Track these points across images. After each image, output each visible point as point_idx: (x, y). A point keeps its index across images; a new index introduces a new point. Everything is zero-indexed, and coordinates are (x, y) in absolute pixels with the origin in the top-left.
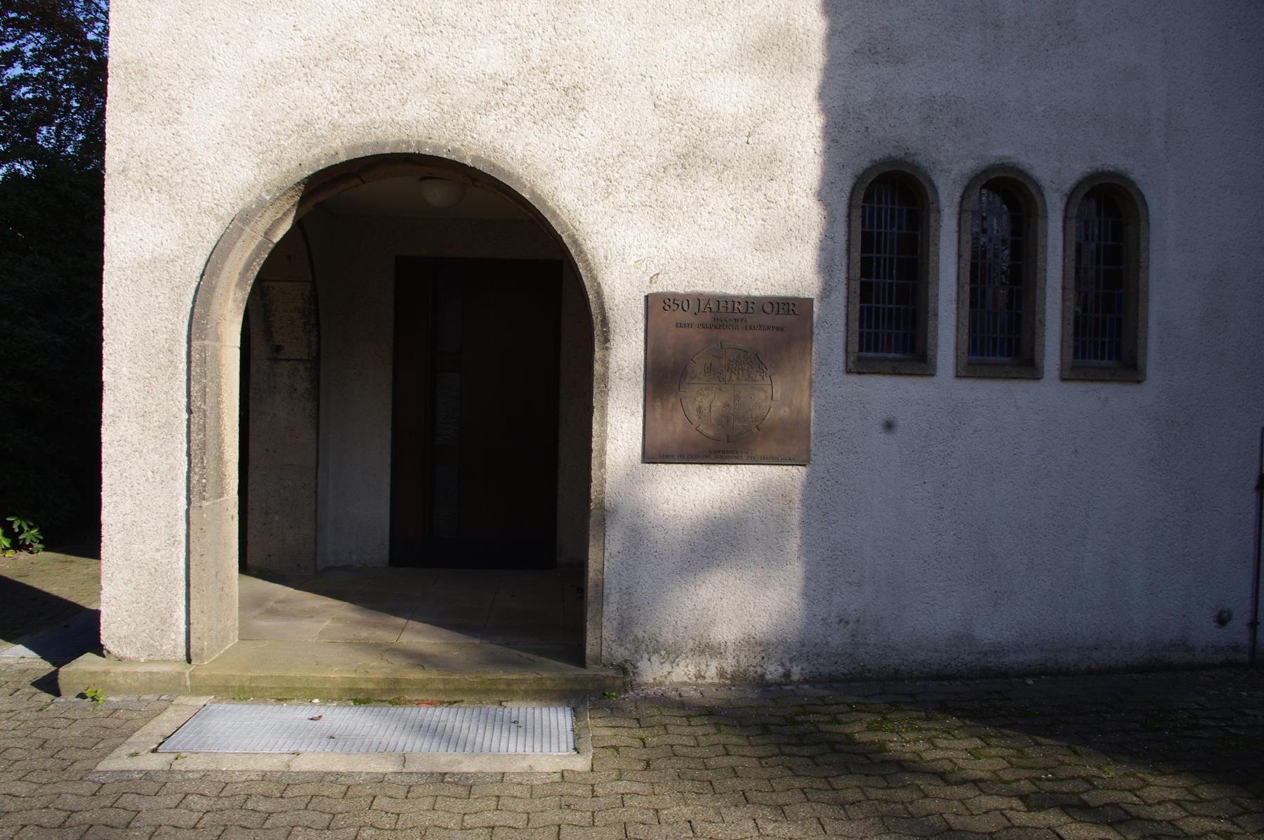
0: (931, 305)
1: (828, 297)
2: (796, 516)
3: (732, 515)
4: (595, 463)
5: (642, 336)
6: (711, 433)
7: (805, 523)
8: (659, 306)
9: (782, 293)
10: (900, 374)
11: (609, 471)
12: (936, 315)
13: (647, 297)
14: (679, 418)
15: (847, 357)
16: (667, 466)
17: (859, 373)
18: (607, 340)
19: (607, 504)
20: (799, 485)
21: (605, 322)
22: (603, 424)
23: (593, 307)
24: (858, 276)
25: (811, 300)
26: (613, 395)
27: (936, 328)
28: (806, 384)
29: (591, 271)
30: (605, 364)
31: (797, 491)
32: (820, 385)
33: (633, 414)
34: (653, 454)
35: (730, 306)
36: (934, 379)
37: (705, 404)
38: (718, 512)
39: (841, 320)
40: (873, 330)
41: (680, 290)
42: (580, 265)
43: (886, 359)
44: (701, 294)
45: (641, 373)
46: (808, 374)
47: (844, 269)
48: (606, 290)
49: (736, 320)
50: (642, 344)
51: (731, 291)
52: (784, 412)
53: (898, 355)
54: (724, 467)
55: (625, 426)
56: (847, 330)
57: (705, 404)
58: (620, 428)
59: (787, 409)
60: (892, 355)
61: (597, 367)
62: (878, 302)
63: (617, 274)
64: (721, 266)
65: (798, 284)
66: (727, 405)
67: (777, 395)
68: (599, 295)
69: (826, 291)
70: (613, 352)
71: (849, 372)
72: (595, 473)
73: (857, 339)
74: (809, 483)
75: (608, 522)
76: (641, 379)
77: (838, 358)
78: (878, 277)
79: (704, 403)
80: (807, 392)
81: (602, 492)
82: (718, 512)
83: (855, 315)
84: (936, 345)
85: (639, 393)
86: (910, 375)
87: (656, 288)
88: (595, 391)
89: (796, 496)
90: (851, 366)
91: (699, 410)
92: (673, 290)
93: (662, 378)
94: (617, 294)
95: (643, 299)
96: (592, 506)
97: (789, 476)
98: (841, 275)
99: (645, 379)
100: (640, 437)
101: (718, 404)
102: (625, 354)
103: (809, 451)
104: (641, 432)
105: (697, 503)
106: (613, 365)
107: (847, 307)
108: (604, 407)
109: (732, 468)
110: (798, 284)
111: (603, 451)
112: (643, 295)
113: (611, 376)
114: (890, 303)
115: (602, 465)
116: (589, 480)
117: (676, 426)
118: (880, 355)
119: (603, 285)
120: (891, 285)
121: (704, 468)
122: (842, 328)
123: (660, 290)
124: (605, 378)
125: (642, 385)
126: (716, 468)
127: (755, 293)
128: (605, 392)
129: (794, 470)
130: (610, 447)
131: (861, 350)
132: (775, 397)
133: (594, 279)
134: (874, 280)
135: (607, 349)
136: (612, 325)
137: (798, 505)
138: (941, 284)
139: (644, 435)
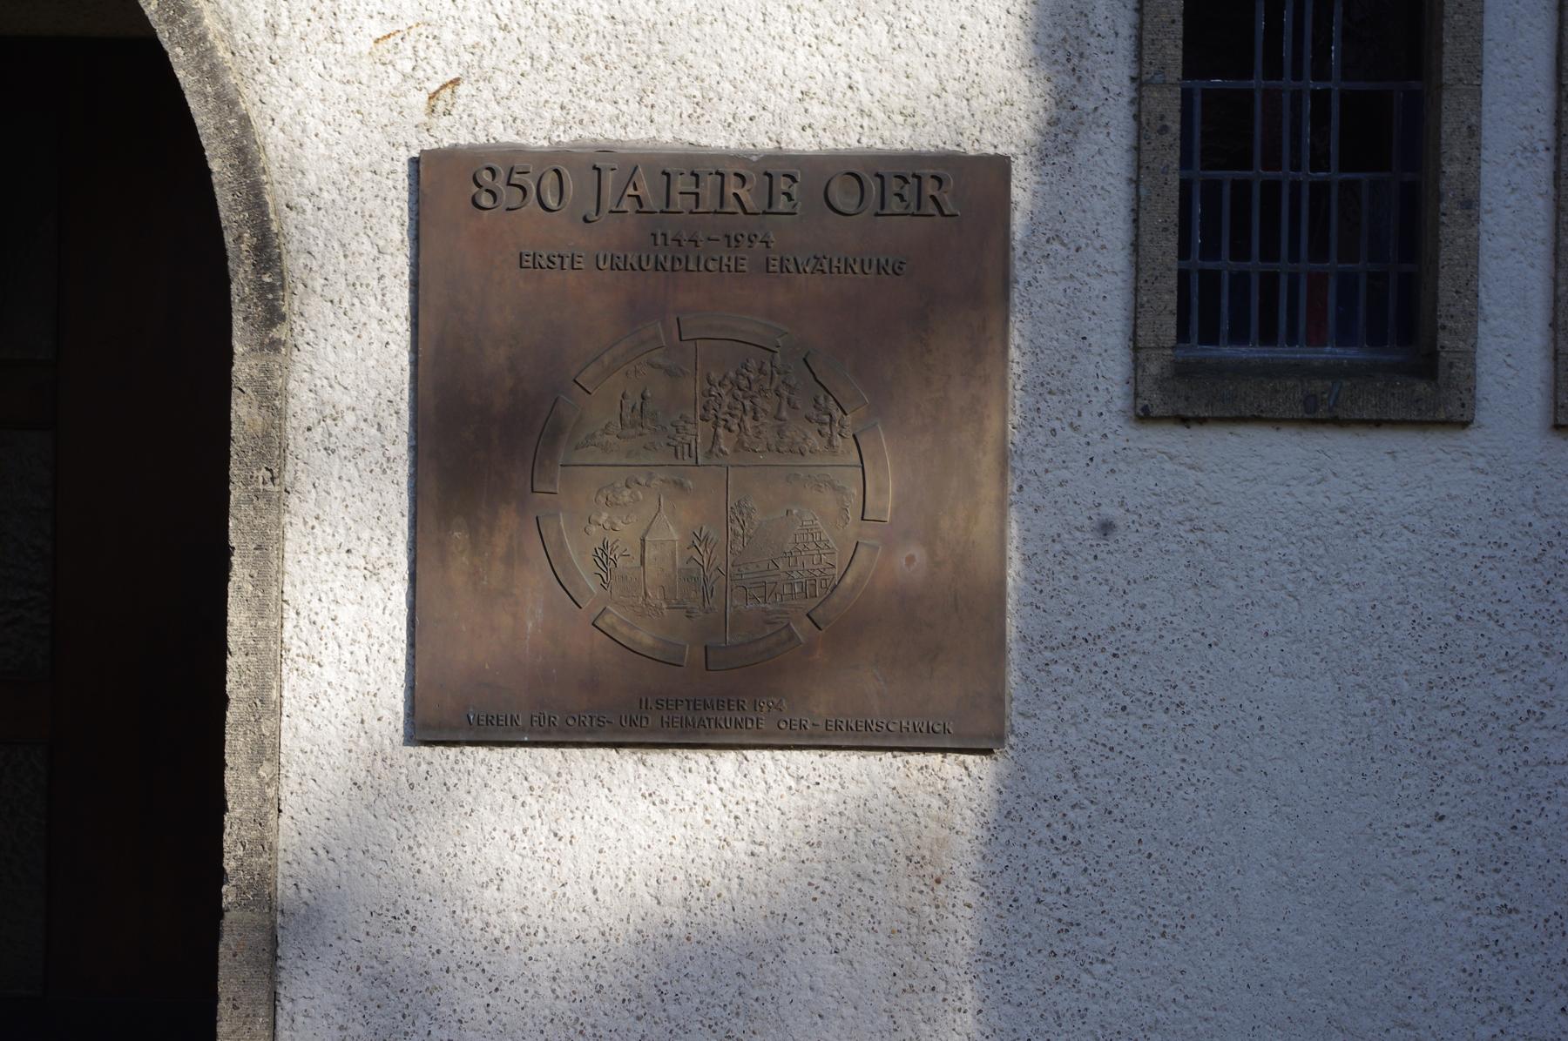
0: (1451, 169)
1: (1067, 149)
2: (962, 924)
3: (727, 929)
4: (236, 746)
5: (401, 300)
6: (645, 637)
7: (994, 962)
8: (459, 195)
9: (899, 138)
10: (1337, 422)
11: (292, 771)
12: (1470, 204)
13: (415, 162)
14: (534, 582)
15: (1137, 364)
16: (495, 755)
17: (1185, 421)
18: (274, 316)
19: (284, 890)
20: (968, 823)
21: (267, 252)
22: (269, 606)
23: (224, 199)
24: (1175, 72)
25: (999, 167)
26: (300, 508)
27: (1472, 252)
28: (987, 461)
29: (214, 73)
30: (272, 399)
31: (962, 844)
32: (1049, 457)
33: (372, 572)
34: (452, 709)
35: (709, 182)
36: (1470, 439)
37: (626, 532)
38: (676, 915)
39: (1117, 232)
40: (1255, 266)
41: (537, 136)
42: (179, 57)
43: (1270, 371)
44: (606, 151)
45: (399, 428)
46: (993, 425)
47: (1125, 46)
48: (273, 141)
49: (731, 241)
50: (403, 327)
51: (716, 138)
52: (909, 562)
53: (1350, 354)
54: (699, 758)
55: (347, 614)
56: (1137, 268)
57: (626, 532)
58: (328, 616)
59: (919, 553)
60: (1330, 353)
61: (243, 411)
62: (1296, 167)
63: (311, 82)
64: (679, 48)
65: (958, 107)
66: (698, 540)
67: (885, 502)
68: (246, 157)
69: (1061, 132)
70: (302, 358)
71: (1144, 417)
72: (237, 781)
73: (1171, 301)
74: (1008, 817)
75: (287, 951)
76: (401, 449)
77: (1107, 366)
78: (1273, 69)
79: (626, 533)
80: (989, 491)
81: (264, 846)
82: (676, 915)
83: (1167, 209)
84: (1473, 315)
85: (396, 498)
86: (1378, 424)
87: (452, 133)
88: (236, 493)
89: (962, 854)
90: (1154, 398)
91: (603, 556)
92: (507, 136)
93: (478, 444)
94: (313, 152)
95: (402, 170)
96: (229, 894)
97: (954, 784)
98: (1114, 71)
99: (415, 449)
100: (400, 652)
101: (669, 534)
102: (338, 364)
103: (999, 699)
104: (403, 635)
105: (603, 884)
106: (301, 401)
107: (1136, 182)
108: (268, 548)
109: (727, 761)
110: (958, 107)
111: (267, 705)
112: (404, 156)
113: (297, 441)
114: (1319, 162)
115: (266, 751)
116: (216, 804)
117: (526, 616)
118: (1281, 353)
119: (259, 124)
120: (1321, 99)
121: (625, 763)
122: (1119, 259)
123: (464, 138)
124: (272, 449)
125: (403, 471)
126: (667, 763)
127: (801, 143)
128: (274, 499)
129: (948, 767)
130: (294, 689)
131: (1183, 334)
132: (855, 507)
133: (227, 102)
134: (1257, 83)
135: (275, 345)
136: (294, 264)
137: (967, 893)
138: (1492, 88)
139: (412, 644)
